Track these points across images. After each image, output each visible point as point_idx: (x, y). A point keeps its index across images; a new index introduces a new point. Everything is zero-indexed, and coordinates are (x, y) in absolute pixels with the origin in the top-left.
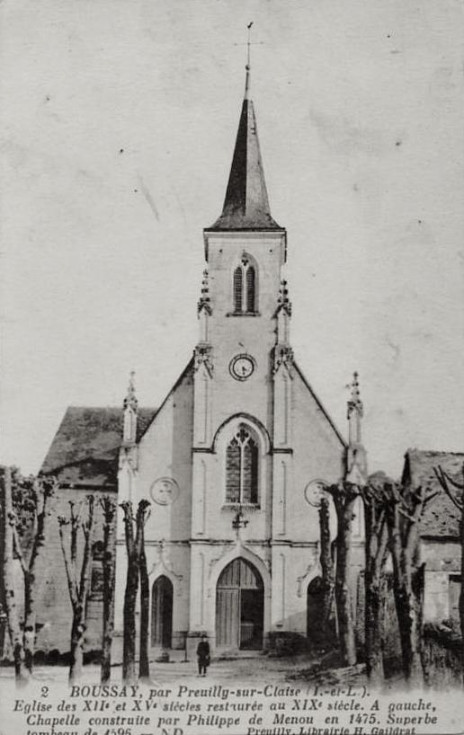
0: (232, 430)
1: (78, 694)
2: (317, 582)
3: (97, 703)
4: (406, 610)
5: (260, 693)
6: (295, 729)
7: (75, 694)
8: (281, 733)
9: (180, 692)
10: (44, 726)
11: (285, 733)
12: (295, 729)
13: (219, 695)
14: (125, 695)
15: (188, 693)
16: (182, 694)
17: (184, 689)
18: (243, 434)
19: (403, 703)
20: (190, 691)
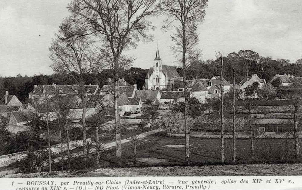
0: (156, 77)
1: (29, 184)
2: (14, 79)
3: (201, 185)
4: (21, 98)
5: (104, 183)
6: (40, 187)
7: (28, 184)
8: (30, 189)
9: (74, 183)
10: (156, 186)
11: (56, 188)
12: (40, 187)
13: (92, 182)
14: (49, 184)
15: (189, 187)
16: (187, 188)
17: (75, 182)
18: (157, 77)
19: (98, 182)
20: (78, 182)
